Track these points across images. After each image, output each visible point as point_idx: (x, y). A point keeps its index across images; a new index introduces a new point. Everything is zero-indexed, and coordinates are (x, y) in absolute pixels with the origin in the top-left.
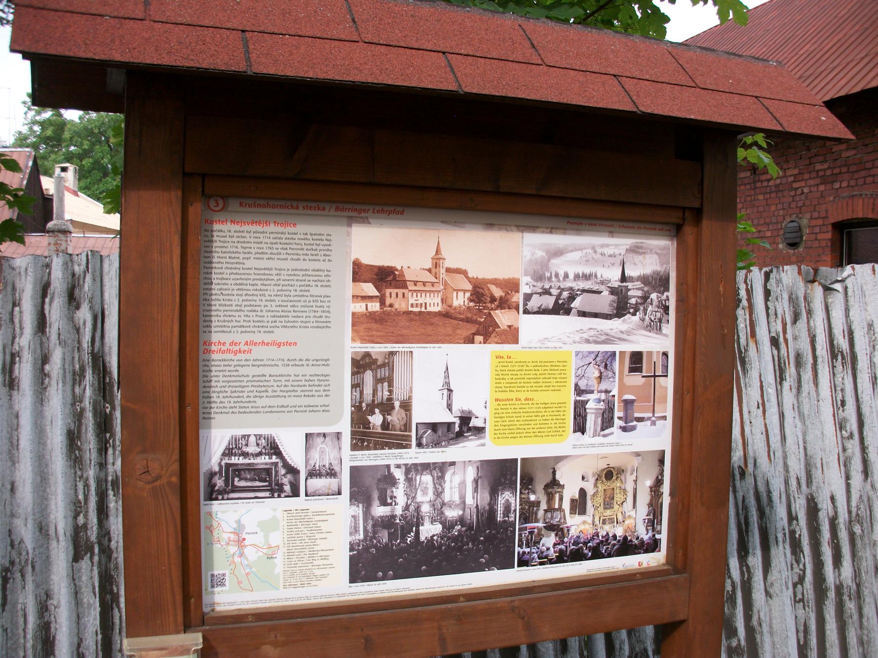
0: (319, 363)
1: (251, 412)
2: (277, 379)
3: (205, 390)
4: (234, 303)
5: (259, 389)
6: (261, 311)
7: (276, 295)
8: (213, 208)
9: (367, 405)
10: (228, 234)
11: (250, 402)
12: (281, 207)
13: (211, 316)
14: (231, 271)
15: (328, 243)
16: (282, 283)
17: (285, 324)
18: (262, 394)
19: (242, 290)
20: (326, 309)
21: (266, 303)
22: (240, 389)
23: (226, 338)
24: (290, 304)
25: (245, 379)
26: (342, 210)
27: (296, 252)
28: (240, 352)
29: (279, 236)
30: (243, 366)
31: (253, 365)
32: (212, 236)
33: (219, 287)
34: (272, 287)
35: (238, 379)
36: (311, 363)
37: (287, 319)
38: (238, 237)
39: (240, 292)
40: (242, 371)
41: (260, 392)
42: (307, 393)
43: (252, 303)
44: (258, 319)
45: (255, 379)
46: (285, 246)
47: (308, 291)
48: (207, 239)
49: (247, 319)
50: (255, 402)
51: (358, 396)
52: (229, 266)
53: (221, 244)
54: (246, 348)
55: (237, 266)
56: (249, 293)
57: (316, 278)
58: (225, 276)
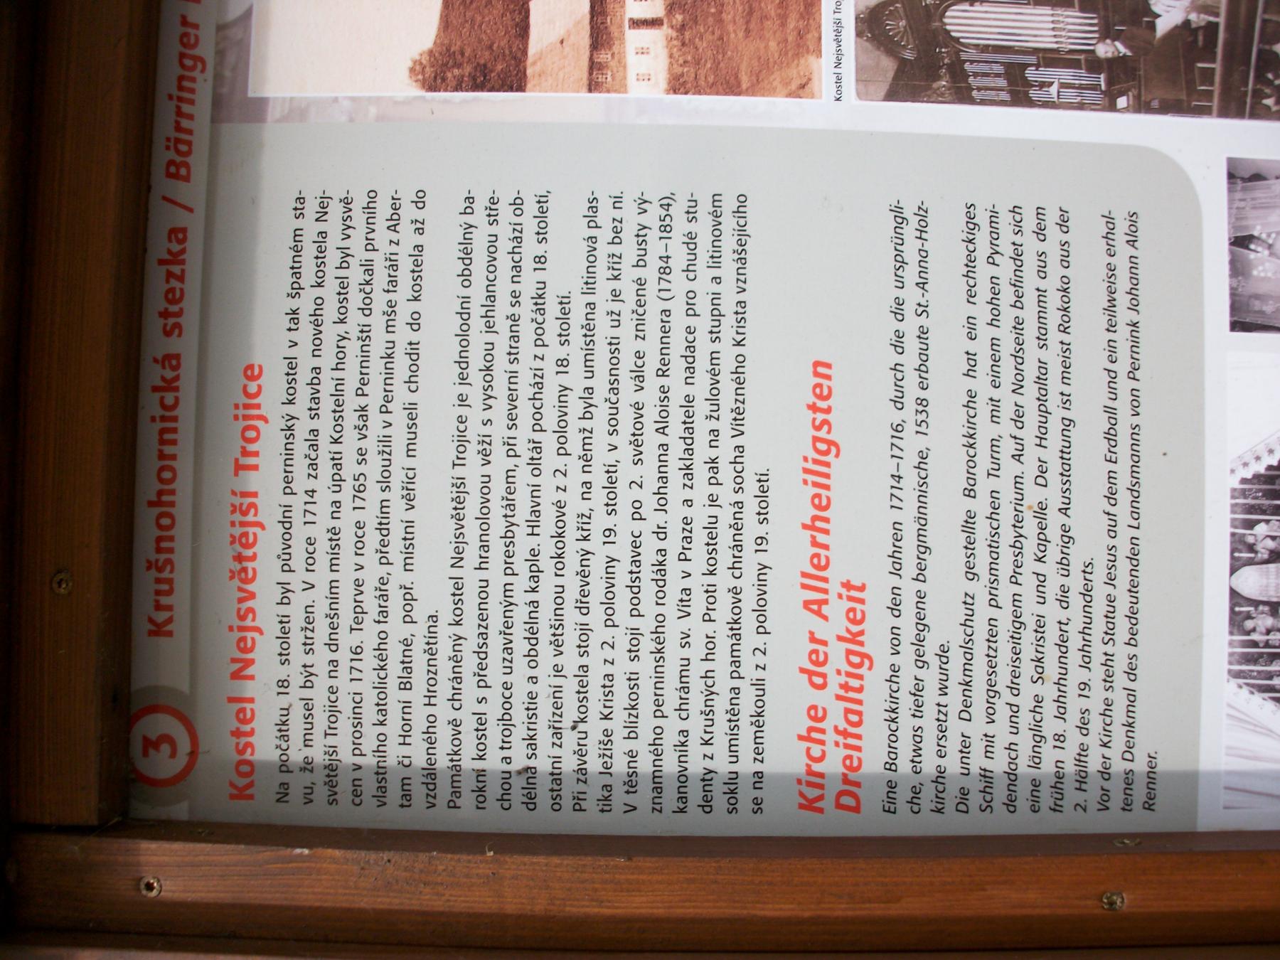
0: (911, 254)
1: (1133, 589)
2: (984, 462)
3: (1023, 804)
4: (623, 666)
5: (1030, 546)
6: (661, 532)
7: (586, 460)
8: (182, 760)
9: (1107, 33)
10: (295, 692)
11: (1087, 593)
12: (166, 437)
13: (656, 778)
14: (469, 682)
15: (336, 210)
16: (524, 432)
17: (726, 416)
18: (1054, 533)
19: (558, 624)
20: (653, 217)
21: (624, 507)
22: (1028, 636)
23: (789, 702)
24: (628, 393)
25: (983, 611)
26: (181, 143)
27: (376, 367)
28: (855, 638)
29: (301, 448)
30: (921, 624)
31: (920, 577)
32: (308, 766)
33: (544, 737)
34: (547, 482)
35: (980, 648)
36: (912, 296)
37: (702, 408)
38: (308, 647)
39: (571, 638)
40: (945, 627)
41: (1043, 542)
42: (1054, 318)
43: (622, 578)
44: (698, 552)
45: (982, 567)
46: (351, 419)
47: (564, 302)
48: (321, 793)
49: (698, 604)
50: (1087, 568)
51: (1066, 75)
52: (444, 689)
53: (345, 725)
54: (837, 609)
55: (444, 648)
56: (572, 594)
57: (504, 263)
58: (493, 711)
